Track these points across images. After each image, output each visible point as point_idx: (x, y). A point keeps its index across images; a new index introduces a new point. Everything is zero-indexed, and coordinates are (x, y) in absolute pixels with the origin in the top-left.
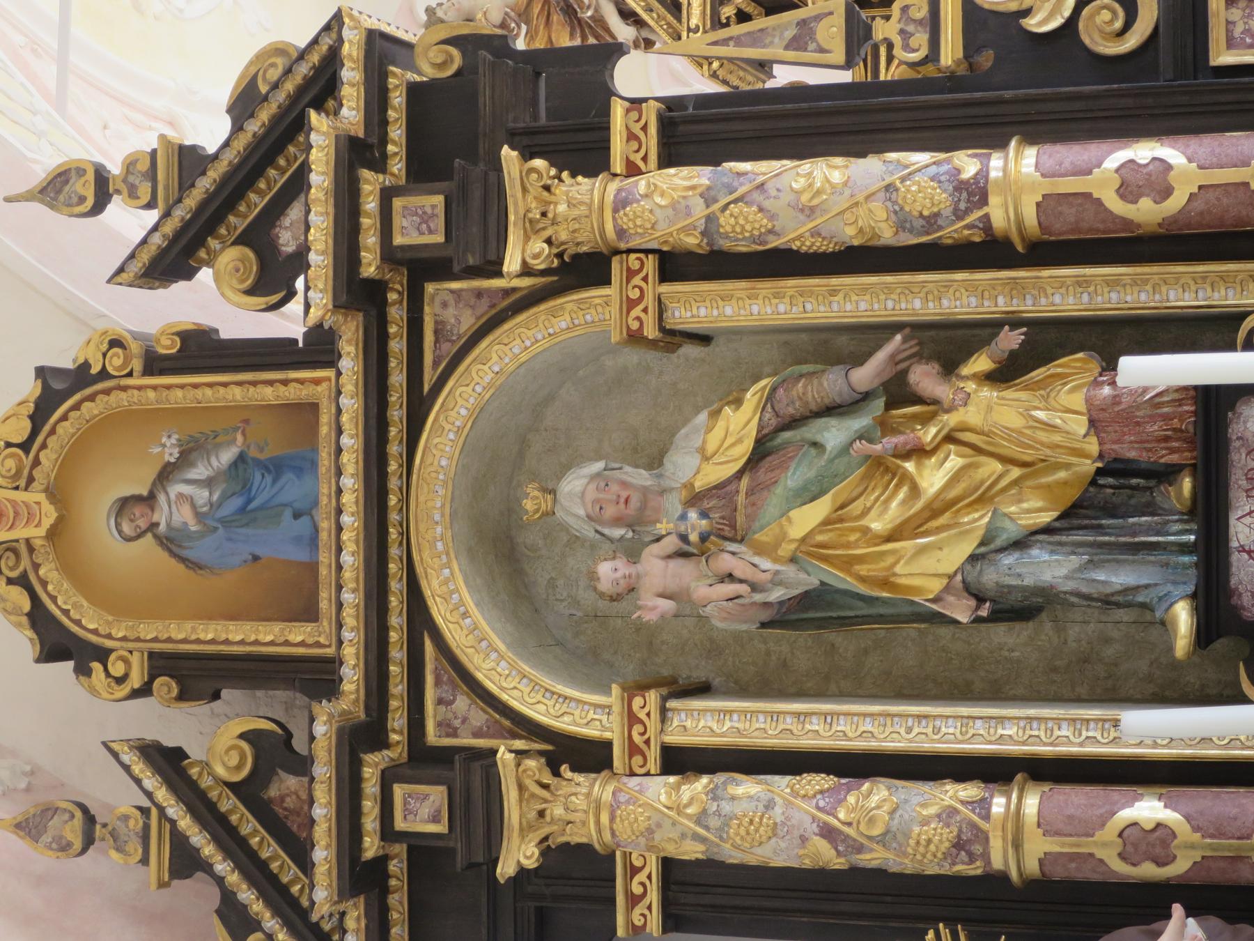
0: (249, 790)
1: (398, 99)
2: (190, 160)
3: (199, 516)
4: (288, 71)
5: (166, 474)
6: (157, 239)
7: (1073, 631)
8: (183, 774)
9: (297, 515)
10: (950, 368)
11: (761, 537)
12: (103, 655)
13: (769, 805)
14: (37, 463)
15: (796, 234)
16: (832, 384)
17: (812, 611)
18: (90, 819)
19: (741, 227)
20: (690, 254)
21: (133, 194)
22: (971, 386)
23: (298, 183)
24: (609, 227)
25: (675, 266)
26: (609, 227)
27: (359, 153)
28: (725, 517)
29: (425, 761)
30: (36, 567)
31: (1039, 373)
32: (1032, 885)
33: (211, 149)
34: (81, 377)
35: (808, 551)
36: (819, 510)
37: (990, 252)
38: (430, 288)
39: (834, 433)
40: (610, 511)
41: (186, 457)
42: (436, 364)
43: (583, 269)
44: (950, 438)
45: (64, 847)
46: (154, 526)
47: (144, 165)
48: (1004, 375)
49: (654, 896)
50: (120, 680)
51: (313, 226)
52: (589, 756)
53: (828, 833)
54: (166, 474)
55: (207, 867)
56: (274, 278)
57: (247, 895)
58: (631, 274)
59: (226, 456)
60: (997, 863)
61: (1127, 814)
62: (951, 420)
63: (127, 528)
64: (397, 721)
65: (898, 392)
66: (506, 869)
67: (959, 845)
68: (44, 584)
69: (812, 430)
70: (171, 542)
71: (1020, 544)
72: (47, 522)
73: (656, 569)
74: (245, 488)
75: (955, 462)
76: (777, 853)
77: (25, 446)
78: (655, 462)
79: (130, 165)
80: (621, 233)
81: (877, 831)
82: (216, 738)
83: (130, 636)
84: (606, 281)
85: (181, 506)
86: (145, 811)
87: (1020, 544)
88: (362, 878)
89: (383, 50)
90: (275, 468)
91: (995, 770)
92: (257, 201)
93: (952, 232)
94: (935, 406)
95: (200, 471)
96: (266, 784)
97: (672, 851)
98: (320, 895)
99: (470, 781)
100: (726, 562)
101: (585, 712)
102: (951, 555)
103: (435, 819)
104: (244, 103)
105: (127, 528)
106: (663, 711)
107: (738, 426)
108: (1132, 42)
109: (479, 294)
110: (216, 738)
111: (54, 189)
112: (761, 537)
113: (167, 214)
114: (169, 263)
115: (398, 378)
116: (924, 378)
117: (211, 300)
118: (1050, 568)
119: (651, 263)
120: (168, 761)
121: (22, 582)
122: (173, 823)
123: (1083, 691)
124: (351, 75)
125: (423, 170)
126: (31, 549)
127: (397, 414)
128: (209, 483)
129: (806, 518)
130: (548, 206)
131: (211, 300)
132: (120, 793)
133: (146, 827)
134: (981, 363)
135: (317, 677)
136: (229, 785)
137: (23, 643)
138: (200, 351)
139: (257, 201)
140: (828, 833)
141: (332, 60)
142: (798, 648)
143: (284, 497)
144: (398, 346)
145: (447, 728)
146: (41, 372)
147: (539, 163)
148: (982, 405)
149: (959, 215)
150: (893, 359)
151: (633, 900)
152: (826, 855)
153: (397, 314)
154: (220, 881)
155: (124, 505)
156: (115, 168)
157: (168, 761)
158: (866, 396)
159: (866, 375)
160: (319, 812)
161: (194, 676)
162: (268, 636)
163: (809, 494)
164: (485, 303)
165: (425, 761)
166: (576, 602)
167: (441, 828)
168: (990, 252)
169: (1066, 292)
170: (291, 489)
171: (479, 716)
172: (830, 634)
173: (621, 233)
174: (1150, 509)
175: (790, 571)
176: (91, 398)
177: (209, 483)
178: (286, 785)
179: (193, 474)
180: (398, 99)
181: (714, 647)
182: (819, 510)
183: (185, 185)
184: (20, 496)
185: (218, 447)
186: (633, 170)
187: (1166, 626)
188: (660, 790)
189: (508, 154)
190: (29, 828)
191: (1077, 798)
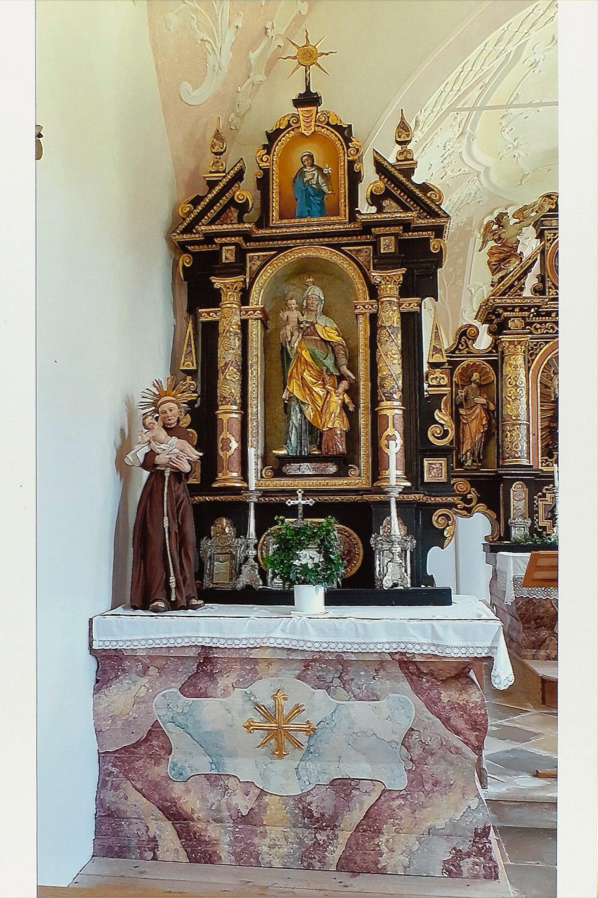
0: (232, 202)
1: (425, 234)
2: (409, 172)
3: (308, 181)
4: (433, 201)
5: (320, 170)
6: (386, 164)
7: (283, 424)
8: (236, 182)
9: (308, 211)
10: (346, 391)
11: (303, 344)
12: (268, 153)
13: (233, 349)
14: (323, 128)
15: (381, 350)
16: (343, 361)
17: (285, 357)
18: (221, 154)
19: (383, 335)
20: (377, 321)
21: (401, 153)
22: (341, 397)
23: (406, 209)
24: (384, 299)
25: (374, 319)
26: (384, 299)
27: (407, 226)
28: (308, 331)
29: (241, 254)
30: (293, 130)
31: (344, 414)
32: (216, 416)
33: (413, 178)
34: (348, 140)
35: (299, 357)
36: (309, 360)
37: (375, 401)
38: (371, 247)
39: (329, 362)
40: (310, 302)
41: (324, 176)
42: (350, 251)
43: (373, 291)
44: (328, 392)
45: (213, 146)
46: (305, 167)
47: (409, 157)
48: (344, 406)
49: (210, 319)
50: (261, 160)
51: (393, 211)
52: (245, 299)
53: (226, 364)
54: (320, 170)
55: (209, 192)
56: (375, 200)
57: (203, 204)
58: (372, 306)
59: (325, 188)
60: (220, 408)
61: (233, 439)
62: (333, 393)
63: (305, 158)
64: (252, 245)
65: (341, 378)
66: (214, 279)
67: (225, 398)
68: (288, 133)
69: (331, 355)
70: (301, 173)
71: (301, 411)
72: (305, 133)
73: (294, 315)
74: (317, 195)
75: (321, 394)
76: (220, 352)
77: (328, 124)
78: (325, 312)
79: (410, 152)
80: (382, 303)
81: (227, 377)
82: (245, 192)
83: (273, 162)
84: (371, 299)
85: (311, 174)
86: (224, 172)
87: (301, 411)
88: (209, 238)
89: (439, 231)
90: (322, 204)
91: (244, 406)
92: (397, 193)
93: (380, 391)
94: (336, 388)
95: (321, 180)
96: (234, 207)
97: (220, 324)
98: (203, 228)
99: (238, 267)
100: (296, 333)
101: (257, 298)
102: (297, 394)
103: (226, 258)
104: (425, 188)
105: (305, 158)
106: (257, 319)
107: (335, 338)
108: (431, 438)
109: (369, 262)
110: (245, 192)
111: (403, 127)
112: (303, 344)
113: (393, 166)
114: (381, 167)
115: (345, 240)
116: (344, 385)
117: (370, 181)
118: (295, 418)
119: (374, 311)
120: (239, 177)
121: (289, 126)
122: (221, 181)
123: (268, 427)
124: (431, 221)
125: (402, 244)
126: (298, 127)
127: (335, 240)
128: (317, 183)
129: (306, 355)
130: (390, 281)
131: (370, 181)
132: (230, 162)
133: (220, 172)
134: (347, 400)
135: (263, 221)
136: (233, 198)
137: (270, 128)
138: (355, 178)
139: (397, 193)
140: (226, 364)
141: (437, 215)
142: (275, 354)
143: (314, 209)
144: (354, 239)
145: (252, 259)
146: (350, 126)
147: (401, 278)
148: (336, 401)
149: (384, 394)
150: (349, 377)
151: (208, 313)
152: (221, 364)
153: (363, 239)
154: (206, 196)
155: (311, 157)
156: (409, 147)
157: (239, 177)
158: (339, 370)
159: (344, 369)
160: (225, 226)
161: (263, 183)
162: (275, 205)
163: (313, 356)
164: (366, 263)
165: (241, 254)
166: (289, 291)
167: (224, 260)
168: (375, 401)
169: (364, 421)
170: (316, 209)
171: (255, 268)
172: (280, 359)
173: (382, 303)
174: (311, 443)
175: (294, 351)
176: (342, 144)
177: (317, 183)
178: (234, 213)
179: (320, 178)
180: (425, 234)
181: (278, 330)
182: (309, 360)
183: (400, 171)
184: (313, 123)
185: (327, 185)
186: (400, 305)
187: (281, 448)
188: (236, 319)
189: (403, 270)
190: (218, 135)
191: (237, 427)
